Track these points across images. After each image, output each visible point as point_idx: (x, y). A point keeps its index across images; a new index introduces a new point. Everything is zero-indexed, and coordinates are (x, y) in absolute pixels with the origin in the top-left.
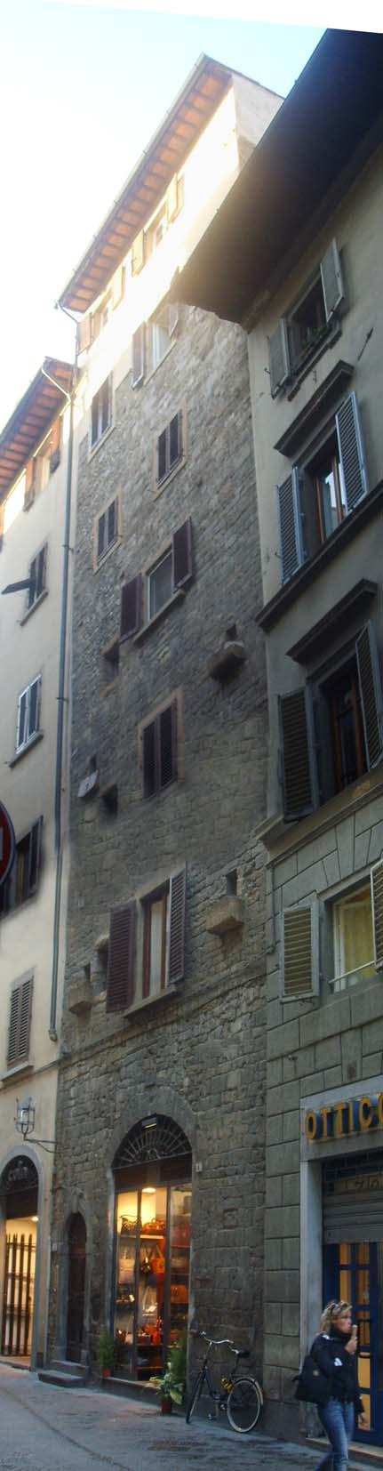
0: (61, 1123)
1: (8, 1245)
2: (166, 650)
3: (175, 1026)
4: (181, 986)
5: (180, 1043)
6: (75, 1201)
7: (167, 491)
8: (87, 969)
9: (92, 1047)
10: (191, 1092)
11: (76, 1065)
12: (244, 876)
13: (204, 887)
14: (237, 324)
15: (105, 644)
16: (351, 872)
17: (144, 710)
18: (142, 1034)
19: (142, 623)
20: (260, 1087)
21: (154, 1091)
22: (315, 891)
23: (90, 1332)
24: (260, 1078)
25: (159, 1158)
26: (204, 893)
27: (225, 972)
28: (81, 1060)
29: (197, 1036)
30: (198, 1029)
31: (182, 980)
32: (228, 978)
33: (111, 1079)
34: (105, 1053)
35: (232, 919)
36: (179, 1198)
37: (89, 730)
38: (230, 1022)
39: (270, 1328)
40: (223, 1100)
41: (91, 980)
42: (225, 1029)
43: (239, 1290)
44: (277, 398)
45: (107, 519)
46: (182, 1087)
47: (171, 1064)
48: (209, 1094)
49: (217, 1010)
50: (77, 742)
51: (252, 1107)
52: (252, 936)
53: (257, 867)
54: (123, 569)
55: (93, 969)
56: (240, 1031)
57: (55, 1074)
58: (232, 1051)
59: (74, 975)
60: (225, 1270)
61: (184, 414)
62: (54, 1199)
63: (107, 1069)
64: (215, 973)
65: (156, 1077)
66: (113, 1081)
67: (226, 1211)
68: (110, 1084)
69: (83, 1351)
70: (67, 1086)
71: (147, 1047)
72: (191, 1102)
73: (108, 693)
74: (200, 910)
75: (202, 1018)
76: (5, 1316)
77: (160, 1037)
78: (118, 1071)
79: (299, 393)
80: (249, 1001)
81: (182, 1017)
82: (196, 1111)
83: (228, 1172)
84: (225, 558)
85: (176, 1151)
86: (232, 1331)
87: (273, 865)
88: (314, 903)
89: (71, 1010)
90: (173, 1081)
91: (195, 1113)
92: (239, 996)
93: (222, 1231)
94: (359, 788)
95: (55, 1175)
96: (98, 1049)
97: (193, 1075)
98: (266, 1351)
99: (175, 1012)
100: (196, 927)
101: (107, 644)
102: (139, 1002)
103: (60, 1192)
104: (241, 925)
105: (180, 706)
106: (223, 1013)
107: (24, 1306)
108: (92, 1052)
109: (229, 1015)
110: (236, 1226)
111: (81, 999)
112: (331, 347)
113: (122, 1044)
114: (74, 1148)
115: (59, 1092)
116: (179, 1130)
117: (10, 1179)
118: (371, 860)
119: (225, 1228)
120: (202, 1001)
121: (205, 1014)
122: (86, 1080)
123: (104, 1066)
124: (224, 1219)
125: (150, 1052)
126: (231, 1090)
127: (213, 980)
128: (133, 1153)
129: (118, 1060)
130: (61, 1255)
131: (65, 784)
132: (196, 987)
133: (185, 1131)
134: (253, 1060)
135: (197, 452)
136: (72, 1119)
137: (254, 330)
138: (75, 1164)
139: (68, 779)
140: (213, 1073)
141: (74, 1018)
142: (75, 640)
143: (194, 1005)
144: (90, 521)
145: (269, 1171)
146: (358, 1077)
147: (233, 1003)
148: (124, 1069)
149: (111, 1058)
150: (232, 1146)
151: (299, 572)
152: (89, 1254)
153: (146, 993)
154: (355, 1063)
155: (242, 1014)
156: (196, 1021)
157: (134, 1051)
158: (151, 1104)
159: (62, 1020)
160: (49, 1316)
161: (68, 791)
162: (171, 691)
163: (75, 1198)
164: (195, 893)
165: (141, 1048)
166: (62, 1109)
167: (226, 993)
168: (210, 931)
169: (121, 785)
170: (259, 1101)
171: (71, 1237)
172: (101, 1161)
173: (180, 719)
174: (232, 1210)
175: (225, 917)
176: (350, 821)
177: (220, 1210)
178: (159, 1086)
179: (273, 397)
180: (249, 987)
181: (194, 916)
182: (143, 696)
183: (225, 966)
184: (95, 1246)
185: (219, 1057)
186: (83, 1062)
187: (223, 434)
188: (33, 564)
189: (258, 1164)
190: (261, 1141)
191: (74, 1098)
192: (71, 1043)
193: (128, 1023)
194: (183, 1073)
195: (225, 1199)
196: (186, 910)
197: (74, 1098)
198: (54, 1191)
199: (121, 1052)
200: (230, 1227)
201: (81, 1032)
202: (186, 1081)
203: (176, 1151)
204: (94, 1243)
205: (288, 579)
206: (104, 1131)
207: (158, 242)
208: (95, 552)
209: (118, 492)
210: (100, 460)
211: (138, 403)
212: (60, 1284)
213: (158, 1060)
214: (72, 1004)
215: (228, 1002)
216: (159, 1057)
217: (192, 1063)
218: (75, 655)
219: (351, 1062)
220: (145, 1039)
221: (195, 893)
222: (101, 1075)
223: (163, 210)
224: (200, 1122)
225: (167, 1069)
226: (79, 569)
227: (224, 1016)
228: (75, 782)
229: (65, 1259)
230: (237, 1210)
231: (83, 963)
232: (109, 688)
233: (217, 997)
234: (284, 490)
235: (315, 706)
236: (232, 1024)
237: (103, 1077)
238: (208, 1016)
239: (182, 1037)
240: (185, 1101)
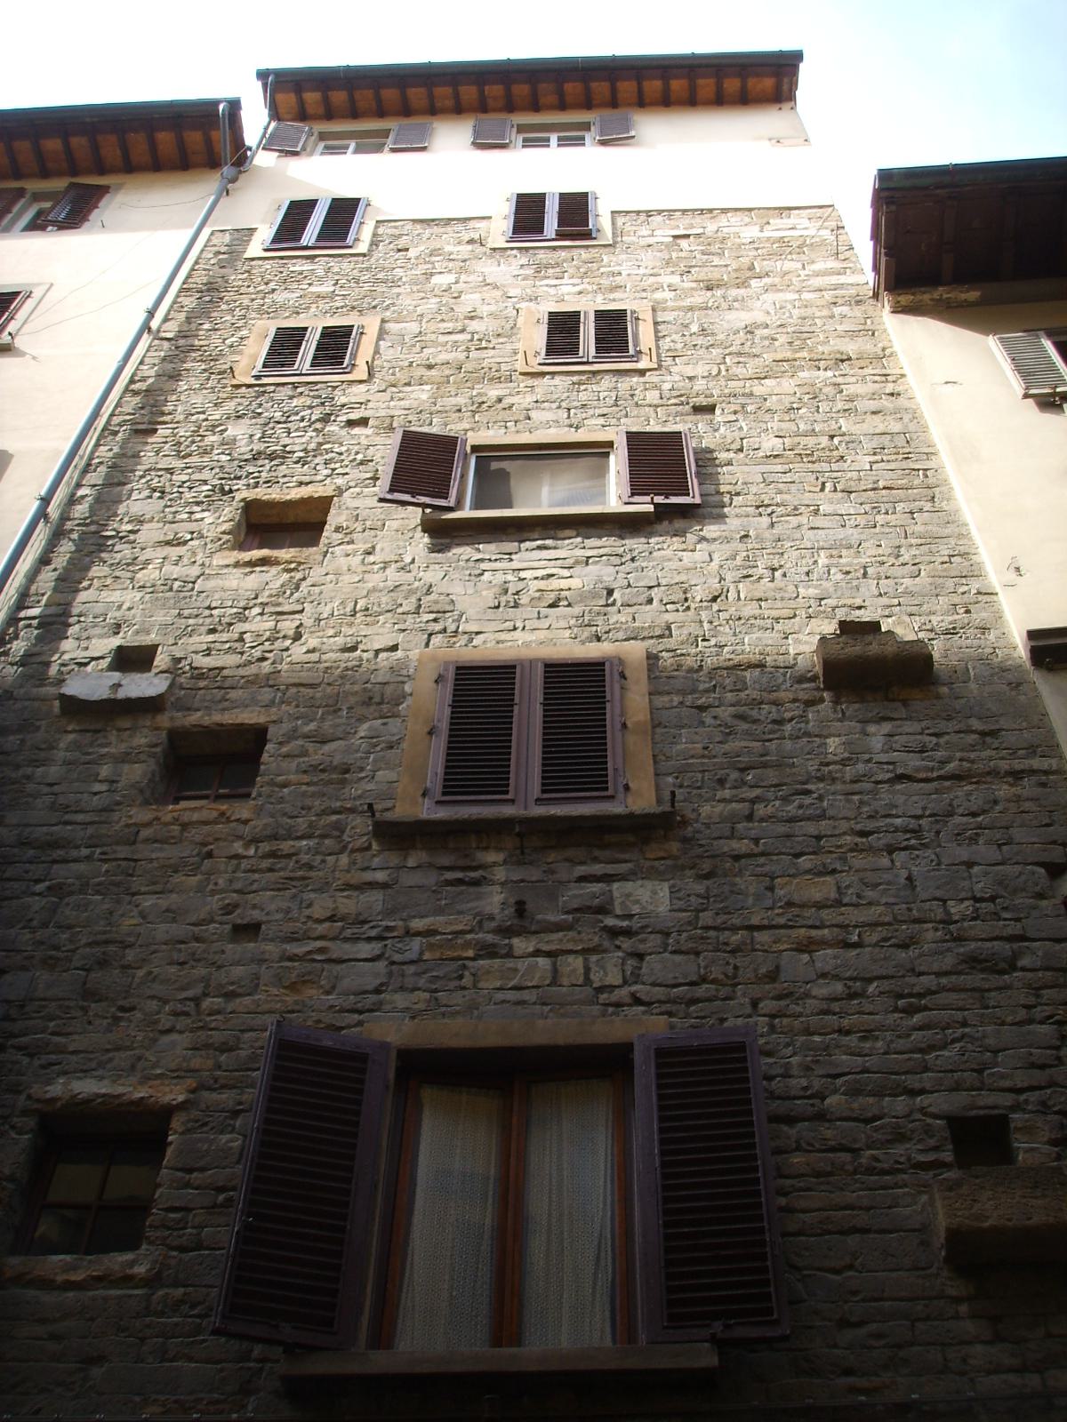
153: (382, 1336)
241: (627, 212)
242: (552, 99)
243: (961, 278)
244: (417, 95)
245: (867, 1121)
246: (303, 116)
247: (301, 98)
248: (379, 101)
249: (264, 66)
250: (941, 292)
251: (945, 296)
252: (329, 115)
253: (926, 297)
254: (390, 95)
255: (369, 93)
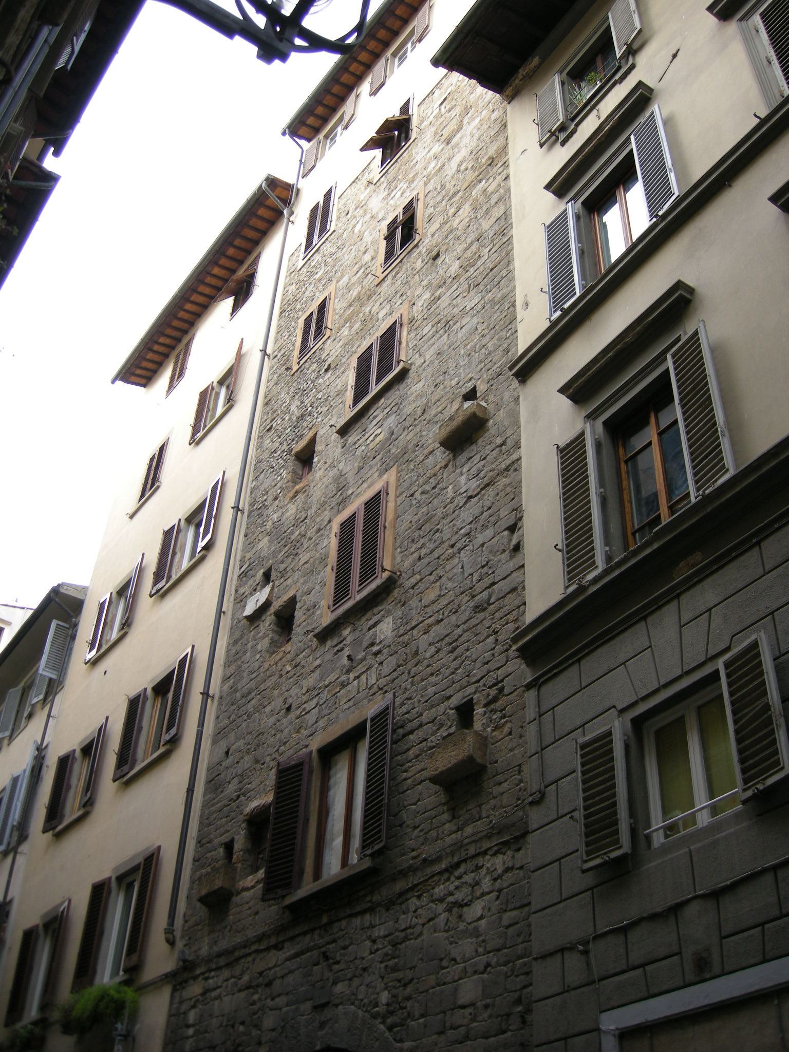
2: (379, 431)
3: (367, 917)
5: (374, 941)
7: (394, 273)
8: (229, 847)
10: (392, 1013)
11: (200, 979)
12: (485, 706)
13: (421, 726)
14: (498, 95)
16: (679, 673)
17: (343, 503)
18: (312, 930)
20: (518, 1001)
21: (328, 1013)
22: (614, 707)
24: (518, 987)
26: (420, 734)
27: (454, 836)
28: (211, 971)
30: (405, 920)
31: (380, 852)
32: (459, 846)
33: (256, 997)
34: (250, 959)
35: (470, 759)
37: (267, 538)
40: (448, 1025)
41: (234, 860)
44: (545, 147)
45: (315, 316)
46: (376, 1005)
48: (422, 1016)
49: (439, 891)
50: (248, 556)
52: (500, 784)
54: (330, 361)
55: (237, 846)
57: (166, 992)
58: (467, 946)
59: (209, 855)
61: (421, 197)
64: (437, 839)
66: (260, 999)
68: (253, 1003)
70: (184, 1007)
71: (320, 948)
72: (390, 1029)
73: (297, 492)
78: (269, 984)
79: (575, 136)
80: (495, 875)
82: (401, 1041)
84: (464, 322)
88: (617, 724)
89: (202, 900)
90: (361, 997)
91: (399, 1045)
92: (478, 868)
97: (394, 987)
99: (368, 899)
100: (406, 779)
102: (307, 887)
106: (451, 894)
109: (459, 896)
111: (218, 883)
112: (620, 83)
113: (278, 947)
115: (170, 1016)
118: (712, 652)
120: (413, 880)
121: (419, 897)
122: (216, 999)
123: (246, 978)
125: (326, 957)
126: (463, 1007)
127: (428, 851)
129: (270, 969)
131: (228, 606)
132: (405, 861)
135: (435, 226)
137: (516, 99)
140: (433, 983)
141: (202, 911)
142: (259, 446)
143: (400, 886)
144: (293, 323)
147: (468, 878)
148: (278, 982)
149: (260, 965)
153: (317, 875)
155: (483, 895)
157: (297, 955)
158: (320, 1033)
159: (185, 915)
161: (229, 614)
162: (380, 476)
164: (404, 736)
165: (308, 950)
167: (457, 865)
168: (434, 780)
169: (302, 596)
173: (390, 507)
175: (460, 757)
176: (672, 607)
178: (336, 1006)
179: (541, 146)
180: (494, 854)
181: (402, 766)
182: (341, 488)
183: (454, 828)
185: (441, 960)
186: (213, 973)
187: (469, 203)
188: (152, 459)
191: (193, 1026)
194: (380, 985)
196: (392, 758)
197: (193, 1026)
199: (275, 957)
202: (384, 997)
205: (559, 313)
207: (399, 65)
208: (296, 353)
209: (332, 288)
210: (313, 264)
211: (364, 202)
213: (336, 967)
214: (204, 892)
216: (338, 963)
217: (395, 969)
218: (259, 461)
220: (316, 937)
221: (404, 736)
222: (240, 991)
223: (412, 33)
225: (350, 979)
226: (274, 373)
227: (451, 899)
228: (241, 601)
231: (225, 838)
233: (440, 873)
234: (556, 230)
236: (465, 909)
240: (382, 1027)
241: (424, 100)
242: (398, 23)
243: (524, 57)
244: (346, 78)
245: (433, 722)
246: (317, 130)
247: (377, 38)
248: (380, 41)
249: (281, 130)
250: (522, 72)
251: (524, 73)
252: (386, 44)
253: (517, 81)
254: (336, 89)
255: (328, 97)
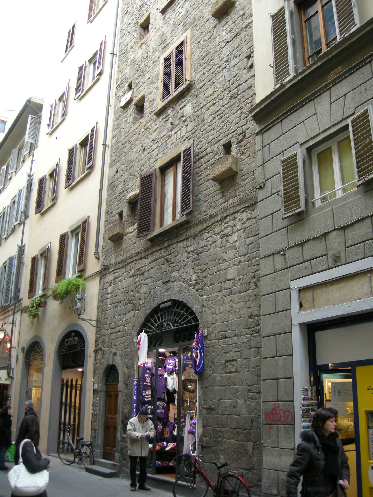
0: (101, 308)
1: (63, 385)
3: (185, 242)
4: (189, 217)
5: (189, 253)
6: (111, 358)
8: (121, 214)
9: (123, 261)
11: (112, 272)
13: (207, 154)
15: (141, 19)
17: (165, 48)
19: (74, 178)
20: (254, 277)
21: (169, 285)
22: (298, 142)
23: (121, 441)
25: (173, 328)
26: (206, 158)
27: (223, 205)
29: (201, 248)
31: (189, 213)
32: (226, 209)
33: (137, 280)
34: (133, 263)
36: (175, 444)
37: (129, 68)
38: (228, 236)
39: (266, 441)
40: (223, 288)
42: (224, 242)
43: (239, 416)
46: (191, 281)
47: (182, 267)
48: (211, 284)
49: (217, 229)
51: (247, 290)
53: (247, 136)
55: (124, 214)
56: (236, 241)
57: (97, 280)
58: (230, 254)
59: (111, 219)
60: (228, 402)
62: (96, 356)
63: (134, 273)
65: (170, 276)
67: (227, 361)
68: (136, 282)
69: (116, 454)
72: (197, 290)
74: (203, 169)
75: (206, 235)
76: (60, 429)
77: (174, 250)
78: (143, 274)
80: (243, 221)
81: (190, 237)
82: (202, 296)
83: (227, 335)
85: (186, 323)
86: (234, 444)
87: (260, 133)
90: (183, 277)
93: (224, 375)
94: (332, 72)
95: (96, 341)
96: (127, 261)
98: (264, 458)
101: (142, 19)
102: (157, 230)
103: (100, 352)
104: (236, 173)
105: (189, 41)
107: (72, 423)
108: (124, 264)
109: (226, 231)
110: (235, 372)
111: (117, 231)
114: (110, 324)
116: (189, 309)
117: (66, 344)
119: (226, 373)
121: (208, 233)
122: (119, 281)
123: (132, 272)
124: (226, 367)
126: (229, 280)
127: (212, 212)
128: (156, 323)
129: (143, 267)
130: (101, 391)
133: (193, 310)
134: (246, 259)
136: (109, 306)
138: (111, 334)
139: (114, 98)
141: (111, 244)
142: (122, 22)
143: (199, 228)
145: (263, 333)
146: (343, 261)
147: (230, 223)
148: (147, 272)
150: (231, 318)
151: (290, 81)
152: (121, 391)
153: (161, 225)
154: (339, 253)
155: (237, 230)
156: (201, 237)
157: (154, 261)
160: (91, 430)
162: (183, 33)
163: (111, 354)
164: (199, 159)
166: (102, 300)
167: (225, 218)
168: (214, 179)
170: (252, 286)
171: (107, 381)
172: (129, 332)
174: (233, 360)
177: (223, 361)
178: (173, 282)
180: (242, 212)
182: (164, 41)
183: (224, 201)
184: (125, 385)
186: (117, 271)
189: (254, 329)
190: (255, 313)
192: (108, 260)
193: (149, 244)
194: (192, 272)
195: (226, 353)
196: (193, 170)
197: (110, 293)
198: (96, 351)
199: (144, 262)
200: (231, 372)
201: (115, 253)
202: (194, 277)
203: (186, 323)
204: (125, 384)
206: (132, 313)
212: (99, 410)
213: (172, 265)
214: (111, 235)
215: (226, 223)
217: (198, 265)
219: (335, 252)
220: (162, 252)
221: (199, 159)
222: (130, 277)
224: (205, 303)
227: (223, 233)
228: (118, 99)
229: (103, 394)
230: (236, 360)
231: (119, 211)
232: (142, 41)
235: (291, 14)
236: (229, 237)
237: (131, 279)
238: (211, 233)
239: (191, 249)
240: (193, 290)
